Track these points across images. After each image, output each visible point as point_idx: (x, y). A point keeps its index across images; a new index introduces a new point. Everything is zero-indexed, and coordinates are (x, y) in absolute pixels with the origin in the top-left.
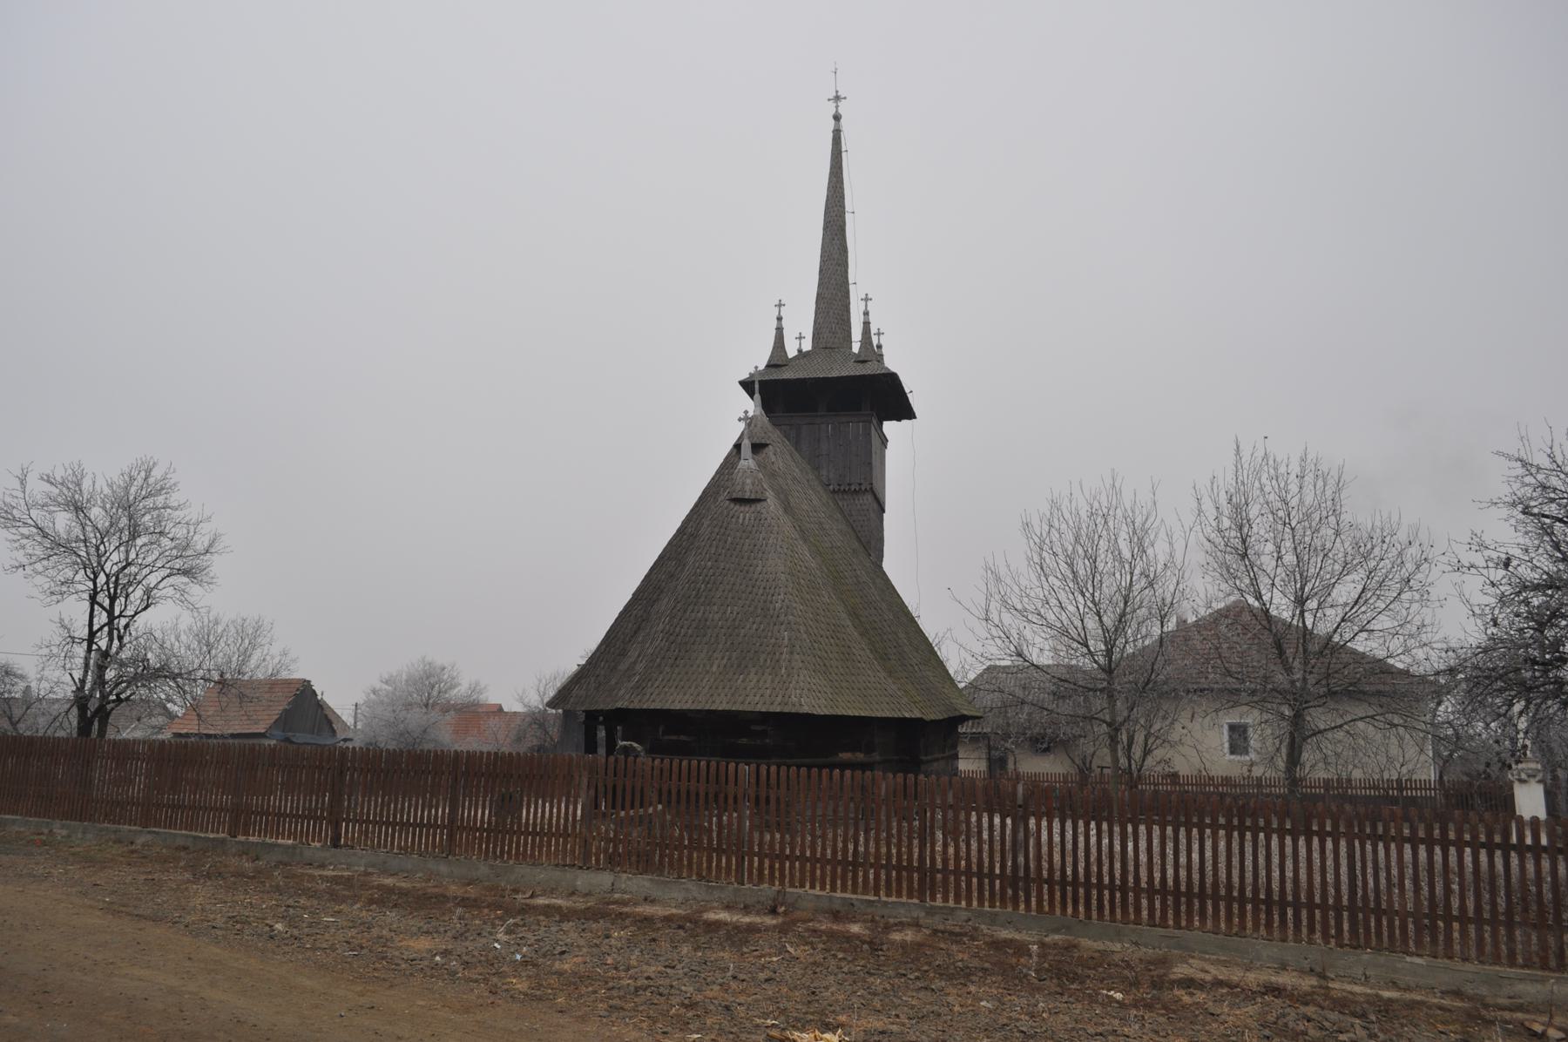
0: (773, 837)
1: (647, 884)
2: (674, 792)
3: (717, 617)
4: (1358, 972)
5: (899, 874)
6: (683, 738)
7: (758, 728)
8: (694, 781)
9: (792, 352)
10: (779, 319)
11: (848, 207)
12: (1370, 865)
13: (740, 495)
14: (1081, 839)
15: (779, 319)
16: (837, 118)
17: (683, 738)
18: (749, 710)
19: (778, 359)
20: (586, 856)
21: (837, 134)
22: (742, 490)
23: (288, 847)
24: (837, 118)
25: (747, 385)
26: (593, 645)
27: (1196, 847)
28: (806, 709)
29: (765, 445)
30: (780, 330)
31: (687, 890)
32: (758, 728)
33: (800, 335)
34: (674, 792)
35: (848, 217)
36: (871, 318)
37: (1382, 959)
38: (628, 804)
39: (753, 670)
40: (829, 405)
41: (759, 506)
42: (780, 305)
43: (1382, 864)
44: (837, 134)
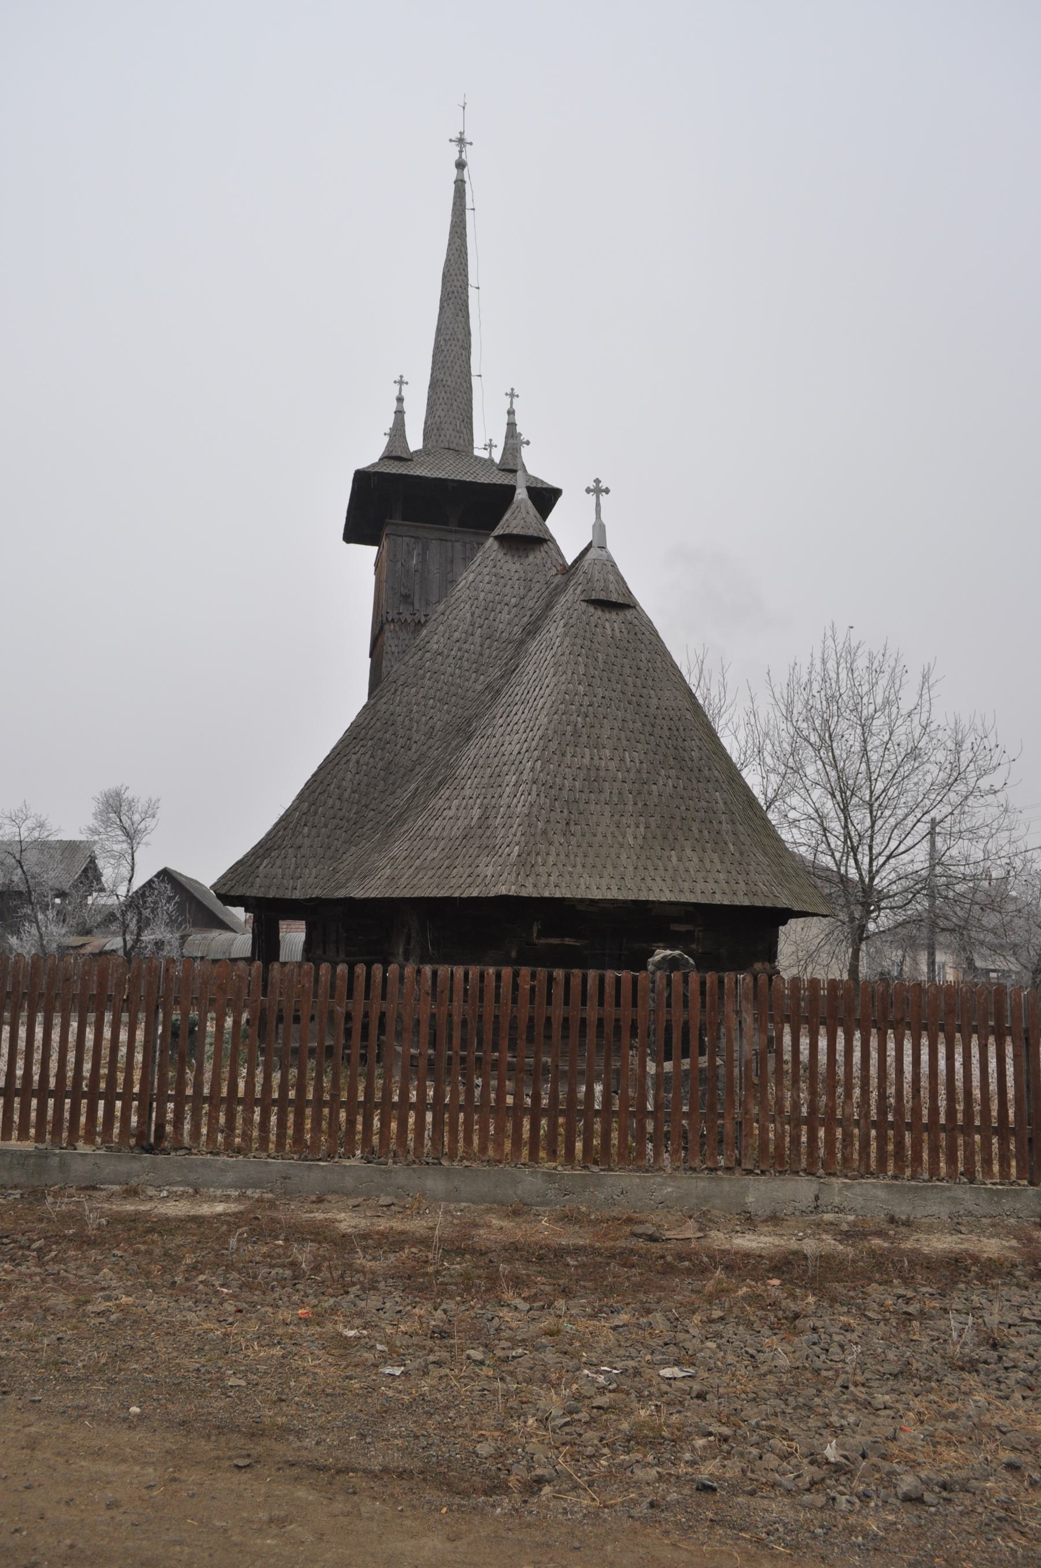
0: (590, 1091)
1: (881, 1194)
2: (505, 1024)
3: (612, 765)
6: (568, 941)
7: (683, 928)
10: (400, 400)
11: (472, 280)
12: (942, 1090)
13: (602, 596)
15: (400, 400)
16: (461, 165)
17: (568, 941)
19: (396, 452)
21: (460, 187)
23: (27, 1155)
24: (461, 165)
30: (400, 413)
31: (955, 1200)
32: (683, 928)
34: (505, 1024)
36: (518, 419)
38: (676, 1050)
39: (688, 845)
42: (401, 382)
43: (121, 1063)
44: (460, 187)
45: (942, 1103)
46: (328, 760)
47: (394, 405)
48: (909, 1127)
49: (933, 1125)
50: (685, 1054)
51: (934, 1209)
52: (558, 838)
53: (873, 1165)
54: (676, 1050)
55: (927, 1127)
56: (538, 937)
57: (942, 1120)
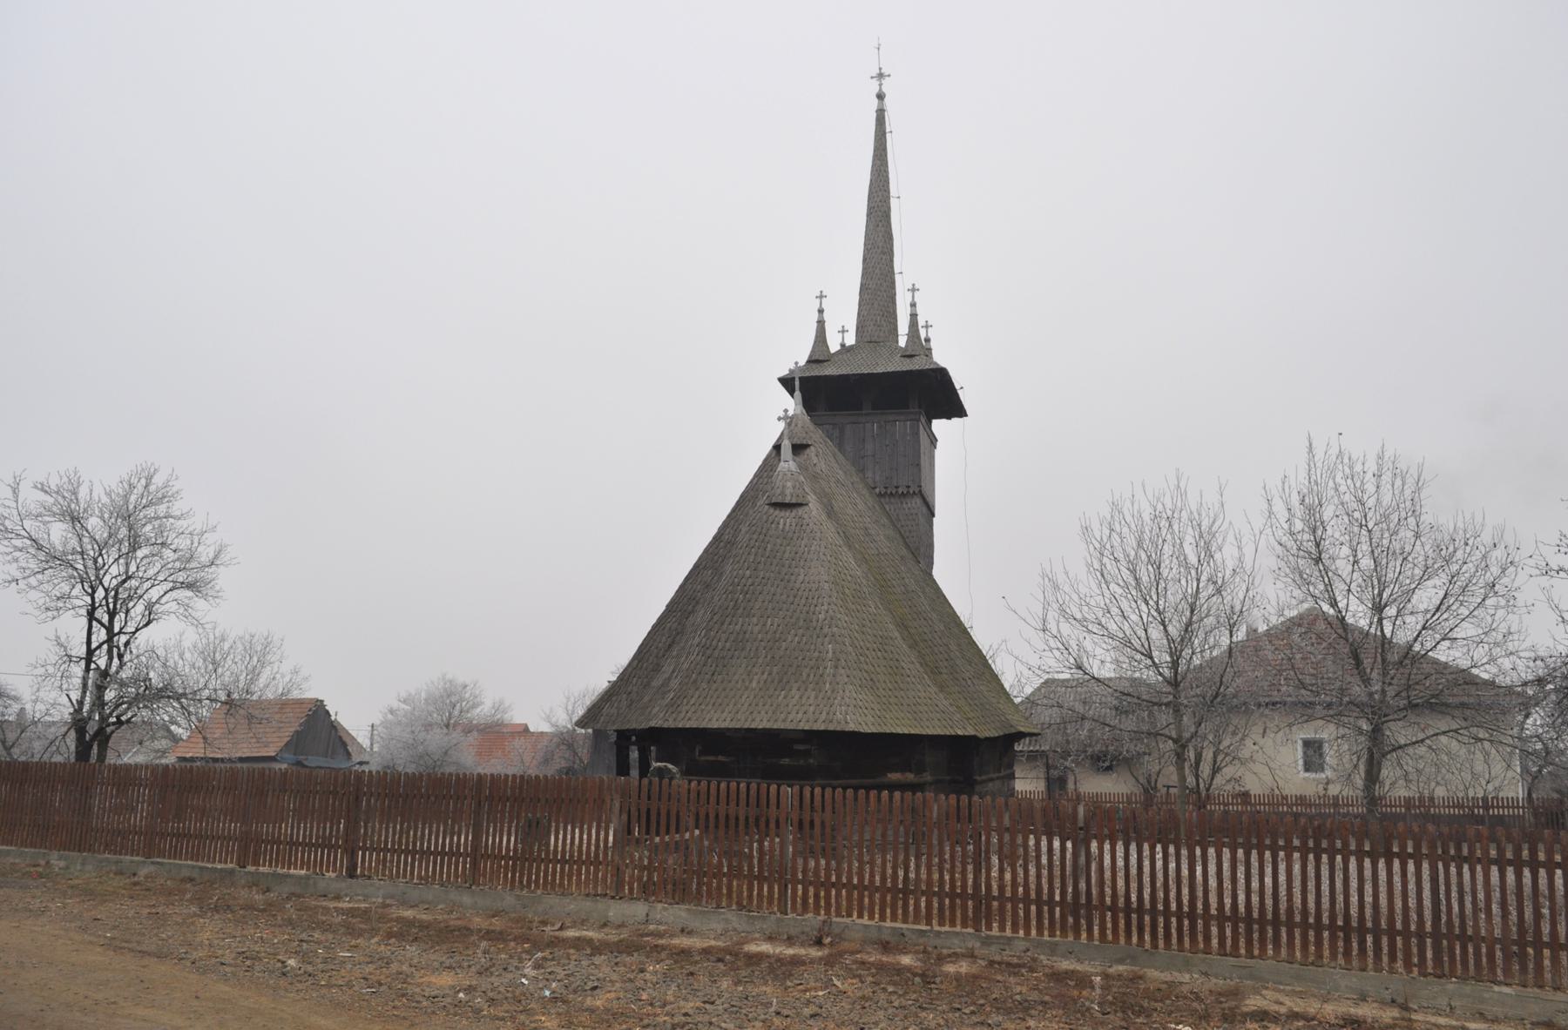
1: (683, 914)
2: (742, 818)
3: (756, 629)
4: (1443, 1002)
6: (721, 758)
7: (801, 747)
9: (834, 347)
10: (821, 311)
13: (780, 500)
15: (821, 311)
16: (881, 96)
17: (721, 758)
18: (794, 733)
19: (820, 355)
20: (619, 886)
22: (783, 494)
24: (881, 96)
25: (787, 382)
28: (852, 727)
29: (807, 446)
30: (821, 324)
31: (727, 921)
32: (801, 747)
33: (843, 329)
35: (893, 203)
37: (1468, 989)
38: (663, 829)
39: (796, 686)
40: (876, 399)
41: (800, 511)
42: (821, 297)
45: (1241, 897)
46: (654, 627)
47: (816, 316)
48: (1458, 937)
49: (1140, 909)
50: (668, 833)
51: (714, 926)
52: (704, 685)
53: (1110, 937)
54: (663, 829)
55: (1458, 937)
56: (701, 753)
57: (970, 891)
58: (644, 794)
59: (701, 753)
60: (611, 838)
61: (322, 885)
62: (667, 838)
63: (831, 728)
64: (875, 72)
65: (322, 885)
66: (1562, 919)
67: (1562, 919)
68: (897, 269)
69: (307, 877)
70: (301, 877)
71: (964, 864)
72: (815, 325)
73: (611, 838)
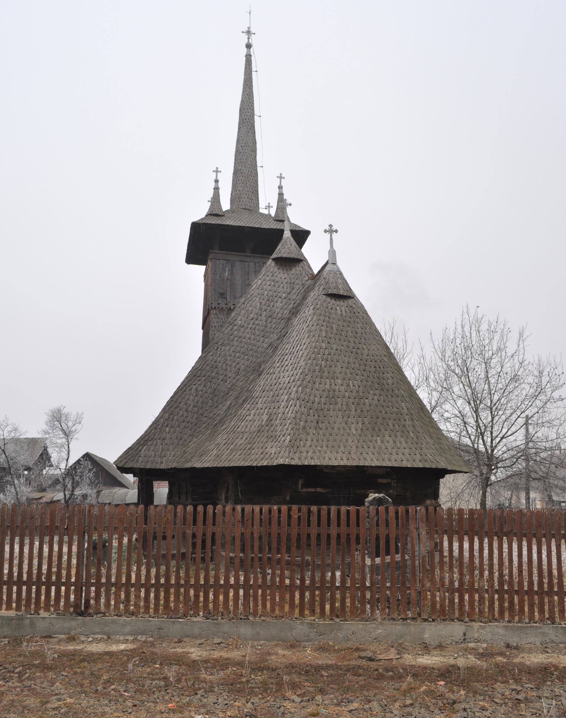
1: (501, 631)
2: (284, 538)
3: (342, 388)
5: (187, 581)
6: (319, 490)
8: (343, 527)
10: (217, 181)
13: (335, 292)
14: (496, 552)
15: (217, 181)
16: (249, 46)
17: (319, 490)
19: (215, 211)
21: (248, 58)
22: (336, 287)
24: (249, 46)
26: (157, 414)
27: (505, 555)
30: (216, 189)
31: (543, 634)
34: (284, 538)
36: (284, 191)
42: (217, 171)
44: (248, 58)
45: (535, 578)
47: (213, 185)
50: (388, 553)
51: (532, 639)
52: (312, 431)
56: (303, 486)
58: (382, 523)
59: (303, 486)
60: (7, 548)
61: (41, 626)
62: (388, 559)
63: (428, 466)
64: (246, 29)
65: (41, 626)
66: (7, 555)
67: (7, 555)
68: (259, 164)
69: (20, 619)
70: (11, 619)
71: (451, 568)
72: (212, 191)
73: (7, 548)
